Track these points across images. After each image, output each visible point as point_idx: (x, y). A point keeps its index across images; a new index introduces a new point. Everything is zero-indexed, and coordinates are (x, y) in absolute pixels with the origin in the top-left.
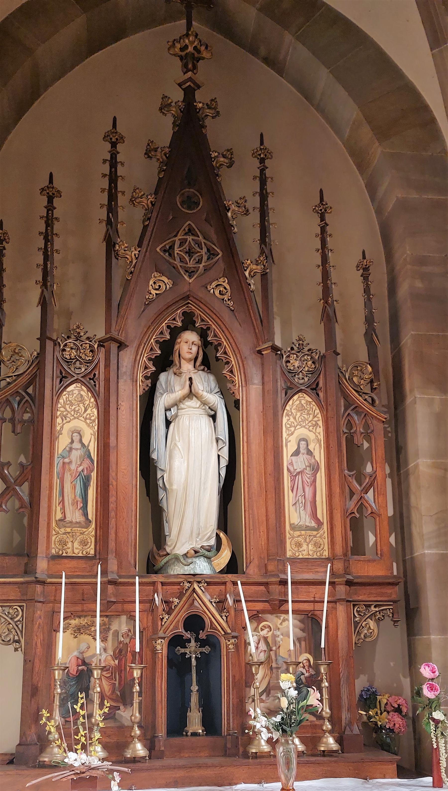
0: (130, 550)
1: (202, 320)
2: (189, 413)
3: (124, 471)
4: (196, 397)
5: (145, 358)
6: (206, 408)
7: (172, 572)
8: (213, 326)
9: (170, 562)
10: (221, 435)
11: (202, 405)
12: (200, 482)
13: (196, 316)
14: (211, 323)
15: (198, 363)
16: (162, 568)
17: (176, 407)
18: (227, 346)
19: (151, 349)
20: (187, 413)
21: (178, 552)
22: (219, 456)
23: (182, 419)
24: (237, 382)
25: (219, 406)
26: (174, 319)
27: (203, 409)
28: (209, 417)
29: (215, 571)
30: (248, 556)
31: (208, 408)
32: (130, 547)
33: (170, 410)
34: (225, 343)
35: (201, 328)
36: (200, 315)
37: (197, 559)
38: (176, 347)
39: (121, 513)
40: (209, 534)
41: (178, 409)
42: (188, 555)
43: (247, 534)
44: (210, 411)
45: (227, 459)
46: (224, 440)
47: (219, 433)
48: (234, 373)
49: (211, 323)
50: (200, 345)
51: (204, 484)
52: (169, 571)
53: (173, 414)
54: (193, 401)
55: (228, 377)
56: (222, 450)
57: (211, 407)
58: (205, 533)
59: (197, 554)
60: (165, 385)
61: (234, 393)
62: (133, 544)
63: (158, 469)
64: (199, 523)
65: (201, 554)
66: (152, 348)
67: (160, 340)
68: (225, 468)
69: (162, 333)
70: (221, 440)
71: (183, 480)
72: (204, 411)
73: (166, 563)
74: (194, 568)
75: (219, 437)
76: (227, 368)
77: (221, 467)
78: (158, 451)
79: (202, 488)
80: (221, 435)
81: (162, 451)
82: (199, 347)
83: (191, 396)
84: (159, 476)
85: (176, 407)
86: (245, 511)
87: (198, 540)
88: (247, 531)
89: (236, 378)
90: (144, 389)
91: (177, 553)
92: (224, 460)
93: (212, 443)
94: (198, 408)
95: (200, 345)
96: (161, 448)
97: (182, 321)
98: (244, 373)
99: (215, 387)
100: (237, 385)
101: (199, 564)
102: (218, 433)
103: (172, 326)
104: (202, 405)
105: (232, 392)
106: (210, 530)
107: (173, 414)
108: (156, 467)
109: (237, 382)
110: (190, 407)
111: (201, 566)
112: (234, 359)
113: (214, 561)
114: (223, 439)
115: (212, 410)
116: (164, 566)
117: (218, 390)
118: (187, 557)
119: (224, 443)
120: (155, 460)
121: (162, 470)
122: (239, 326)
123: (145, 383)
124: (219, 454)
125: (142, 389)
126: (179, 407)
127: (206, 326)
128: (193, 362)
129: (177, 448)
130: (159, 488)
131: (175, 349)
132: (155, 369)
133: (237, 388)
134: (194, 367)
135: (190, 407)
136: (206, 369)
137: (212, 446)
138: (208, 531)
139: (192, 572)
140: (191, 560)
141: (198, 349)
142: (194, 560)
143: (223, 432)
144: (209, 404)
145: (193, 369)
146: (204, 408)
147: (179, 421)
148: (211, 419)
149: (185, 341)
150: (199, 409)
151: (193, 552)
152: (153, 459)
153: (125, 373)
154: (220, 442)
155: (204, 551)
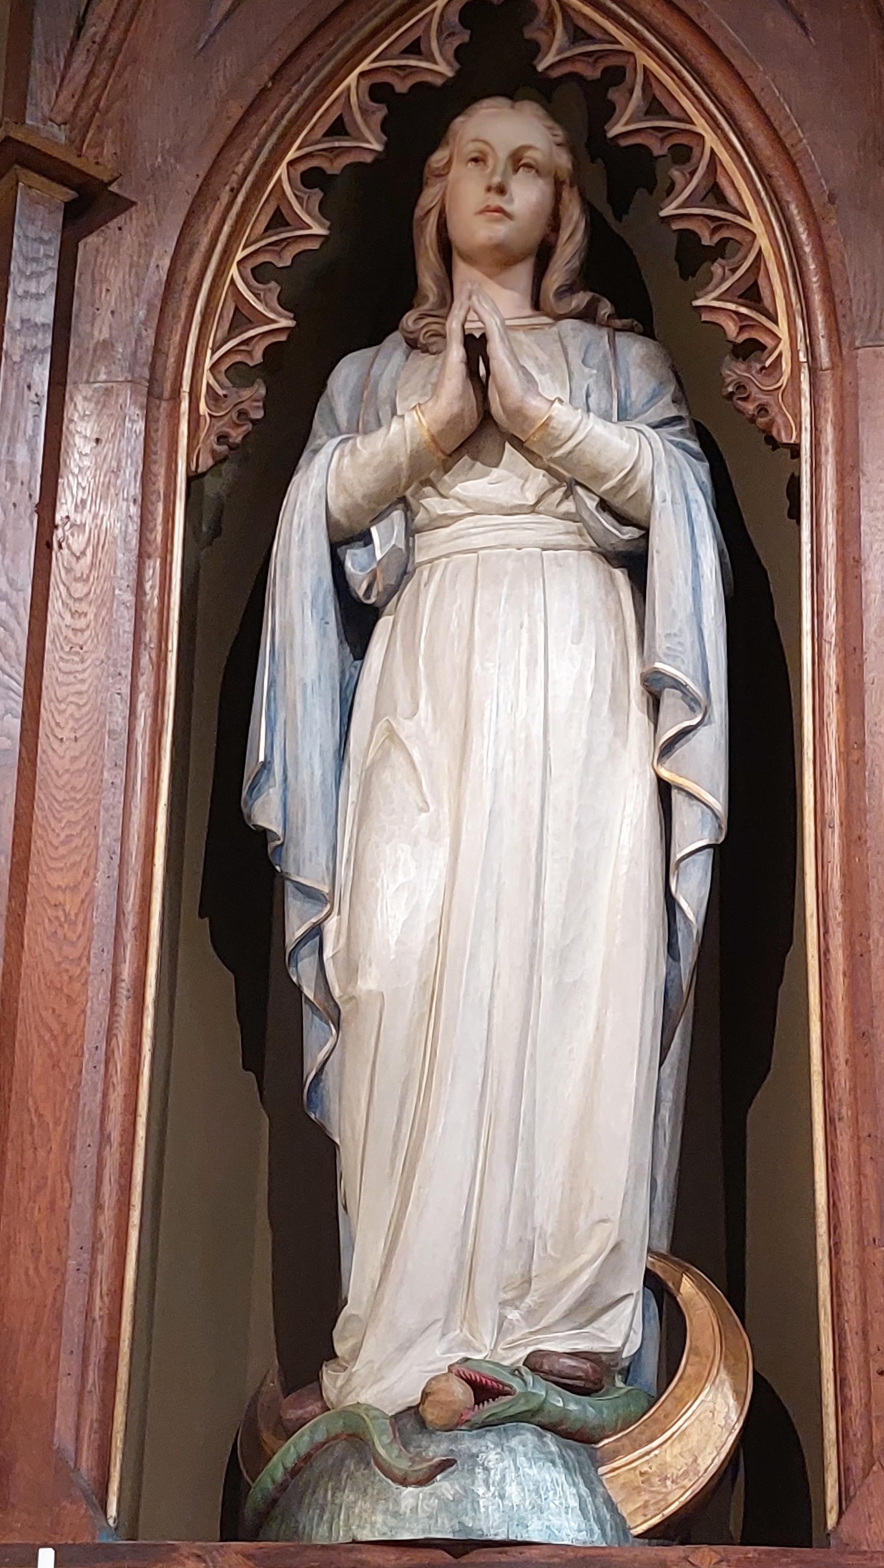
0: (67, 1386)
1: (578, 35)
2: (478, 541)
3: (60, 897)
4: (520, 445)
5: (234, 271)
6: (579, 502)
7: (324, 1529)
8: (644, 59)
9: (318, 1465)
10: (671, 656)
11: (559, 493)
12: (534, 948)
13: (542, 15)
14: (626, 42)
15: (555, 278)
16: (274, 1502)
17: (397, 515)
18: (724, 156)
19: (278, 220)
20: (462, 544)
21: (367, 1396)
22: (664, 790)
23: (433, 586)
24: (784, 347)
25: (663, 490)
26: (415, 49)
27: (566, 517)
28: (603, 565)
29: (626, 1530)
30: (857, 1426)
31: (592, 504)
32: (68, 1363)
33: (365, 539)
34: (711, 141)
35: (572, 75)
36: (780, 355)
37: (490, 1438)
38: (429, 197)
39: (29, 1153)
40: (585, 1277)
41: (411, 532)
42: (430, 1414)
43: (850, 1273)
44: (606, 521)
45: (719, 804)
46: (696, 688)
47: (661, 644)
48: (767, 302)
49: (626, 42)
50: (564, 176)
51: (563, 957)
52: (303, 1519)
53: (379, 555)
54: (496, 473)
55: (731, 328)
56: (682, 750)
57: (617, 502)
58: (565, 1271)
59: (491, 1407)
60: (349, 410)
61: (763, 409)
62: (97, 1346)
63: (289, 887)
64: (527, 1209)
65: (521, 1407)
66: (278, 212)
67: (324, 164)
68: (704, 861)
69: (338, 129)
70: (678, 685)
71: (419, 939)
72: (573, 526)
73: (294, 1472)
74: (457, 1500)
75: (658, 665)
76: (724, 279)
77: (677, 854)
78: (285, 780)
79: (547, 985)
80: (671, 656)
81: (305, 775)
82: (558, 185)
83: (488, 443)
84: (295, 929)
85: (397, 515)
86: (830, 1122)
87: (513, 1315)
88: (849, 1252)
89: (782, 330)
90: (222, 438)
91: (362, 1400)
92: (698, 808)
93: (618, 708)
94: (533, 509)
95: (564, 176)
96: (304, 758)
97: (458, 53)
98: (827, 289)
99: (653, 398)
100: (786, 366)
101: (495, 1476)
102: (652, 647)
103: (401, 87)
104: (559, 493)
105: (750, 408)
106: (593, 1247)
107: (379, 555)
108: (284, 877)
109: (784, 347)
110: (480, 509)
111: (512, 1490)
112: (768, 224)
113: (614, 1455)
114: (692, 685)
115: (622, 519)
116: (283, 1487)
117: (673, 412)
118: (422, 1424)
119: (692, 702)
120: (276, 837)
121: (310, 894)
122: (792, 31)
123: (231, 402)
124: (665, 774)
125: (208, 441)
126: (421, 518)
127: (601, 65)
128: (523, 273)
129: (397, 757)
130: (306, 1008)
131: (418, 212)
132: (291, 323)
133: (784, 379)
134: (536, 305)
135: (480, 509)
136: (606, 309)
137: (621, 733)
138: (585, 1257)
139: (443, 1530)
140: (444, 1447)
141: (557, 198)
142: (467, 1443)
143: (689, 638)
144: (603, 477)
145: (528, 311)
146: (569, 506)
147: (417, 595)
148: (620, 576)
149: (470, 149)
150: (543, 518)
151: (461, 1392)
152: (264, 832)
153: (107, 345)
154: (670, 699)
155: (540, 1389)
